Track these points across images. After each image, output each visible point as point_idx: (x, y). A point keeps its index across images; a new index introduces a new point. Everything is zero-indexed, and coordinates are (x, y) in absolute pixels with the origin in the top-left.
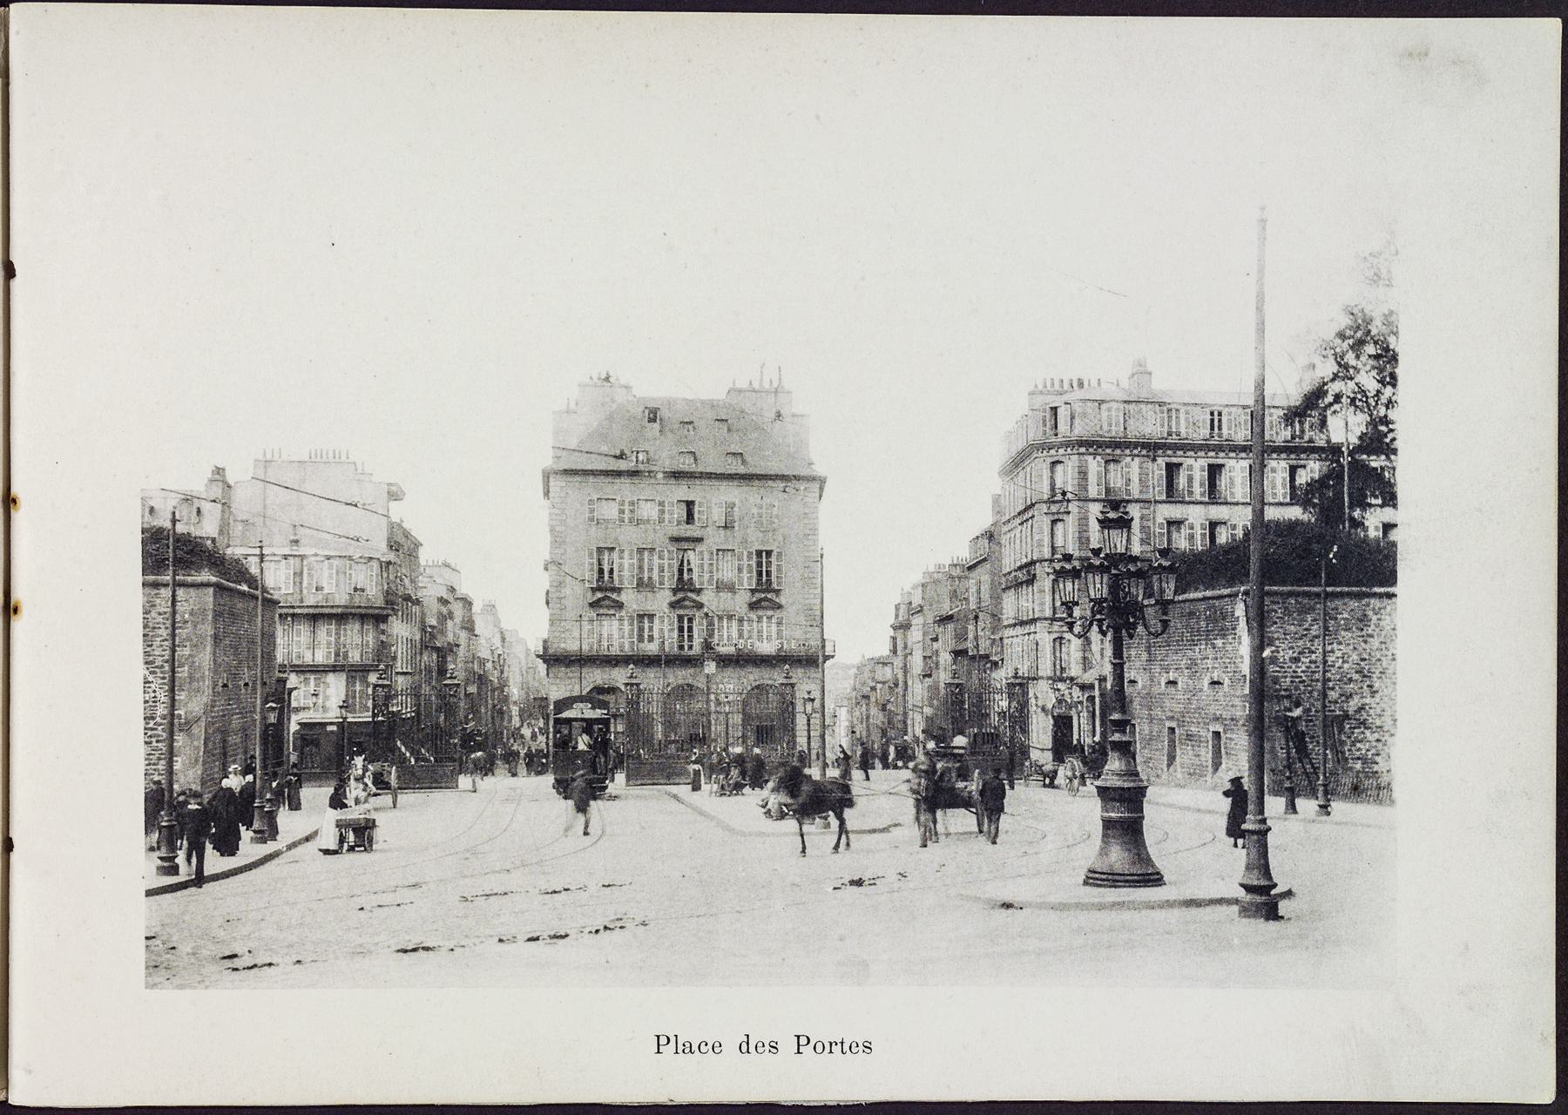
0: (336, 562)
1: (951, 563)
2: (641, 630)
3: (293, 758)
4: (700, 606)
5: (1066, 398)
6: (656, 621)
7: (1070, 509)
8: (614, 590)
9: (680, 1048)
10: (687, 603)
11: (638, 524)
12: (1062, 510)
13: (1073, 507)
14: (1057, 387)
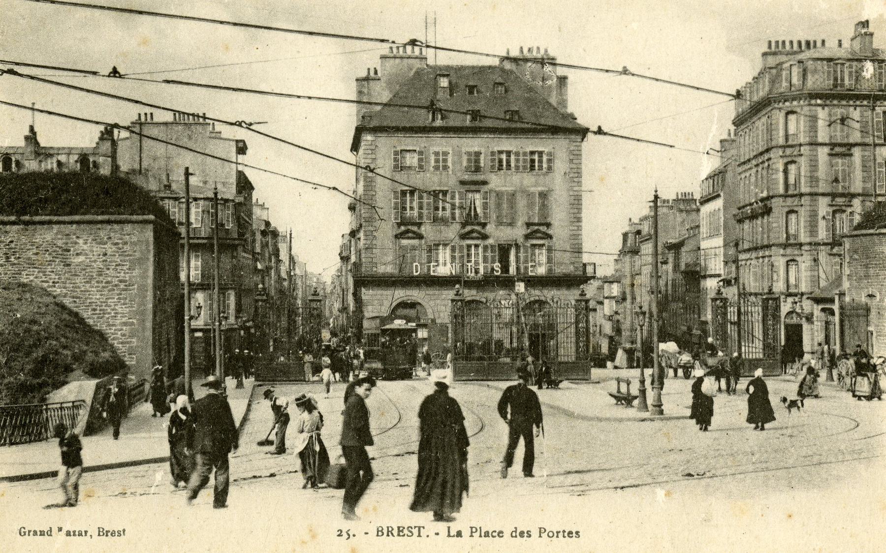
0: (201, 203)
1: (675, 197)
3: (271, 349)
7: (802, 152)
9: (483, 534)
10: (474, 235)
11: (401, 170)
12: (795, 153)
13: (805, 150)
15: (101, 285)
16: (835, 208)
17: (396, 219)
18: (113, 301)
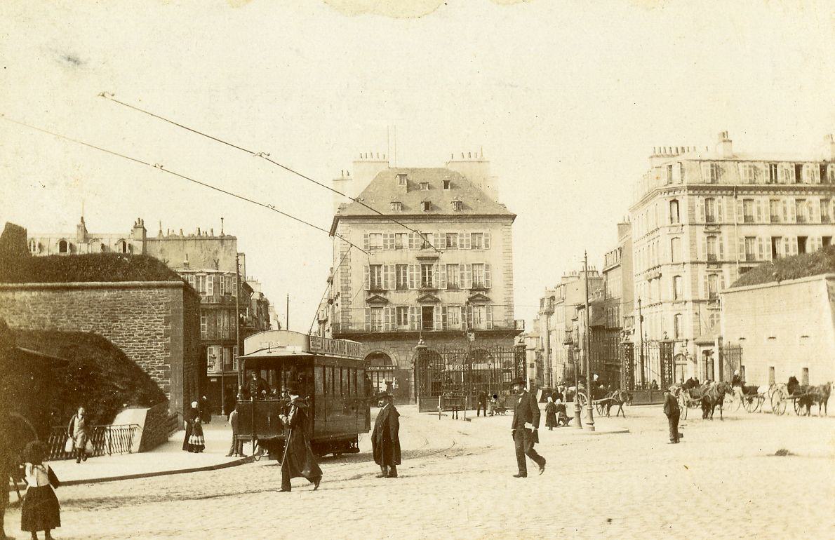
2: (399, 316)
4: (437, 301)
5: (679, 158)
6: (409, 311)
8: (381, 291)
14: (668, 153)
15: (141, 337)
16: (710, 273)
17: (367, 287)
18: (152, 349)
